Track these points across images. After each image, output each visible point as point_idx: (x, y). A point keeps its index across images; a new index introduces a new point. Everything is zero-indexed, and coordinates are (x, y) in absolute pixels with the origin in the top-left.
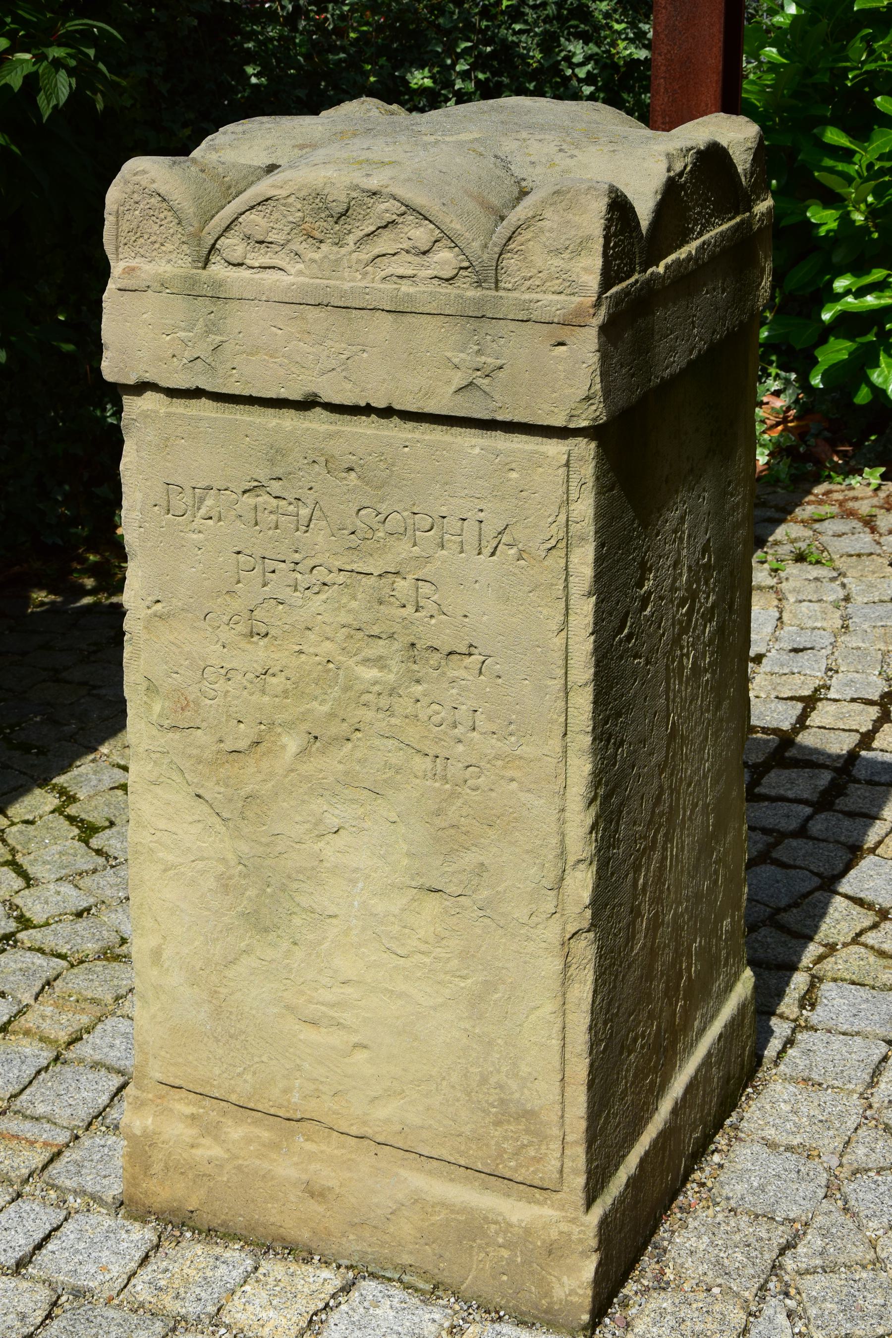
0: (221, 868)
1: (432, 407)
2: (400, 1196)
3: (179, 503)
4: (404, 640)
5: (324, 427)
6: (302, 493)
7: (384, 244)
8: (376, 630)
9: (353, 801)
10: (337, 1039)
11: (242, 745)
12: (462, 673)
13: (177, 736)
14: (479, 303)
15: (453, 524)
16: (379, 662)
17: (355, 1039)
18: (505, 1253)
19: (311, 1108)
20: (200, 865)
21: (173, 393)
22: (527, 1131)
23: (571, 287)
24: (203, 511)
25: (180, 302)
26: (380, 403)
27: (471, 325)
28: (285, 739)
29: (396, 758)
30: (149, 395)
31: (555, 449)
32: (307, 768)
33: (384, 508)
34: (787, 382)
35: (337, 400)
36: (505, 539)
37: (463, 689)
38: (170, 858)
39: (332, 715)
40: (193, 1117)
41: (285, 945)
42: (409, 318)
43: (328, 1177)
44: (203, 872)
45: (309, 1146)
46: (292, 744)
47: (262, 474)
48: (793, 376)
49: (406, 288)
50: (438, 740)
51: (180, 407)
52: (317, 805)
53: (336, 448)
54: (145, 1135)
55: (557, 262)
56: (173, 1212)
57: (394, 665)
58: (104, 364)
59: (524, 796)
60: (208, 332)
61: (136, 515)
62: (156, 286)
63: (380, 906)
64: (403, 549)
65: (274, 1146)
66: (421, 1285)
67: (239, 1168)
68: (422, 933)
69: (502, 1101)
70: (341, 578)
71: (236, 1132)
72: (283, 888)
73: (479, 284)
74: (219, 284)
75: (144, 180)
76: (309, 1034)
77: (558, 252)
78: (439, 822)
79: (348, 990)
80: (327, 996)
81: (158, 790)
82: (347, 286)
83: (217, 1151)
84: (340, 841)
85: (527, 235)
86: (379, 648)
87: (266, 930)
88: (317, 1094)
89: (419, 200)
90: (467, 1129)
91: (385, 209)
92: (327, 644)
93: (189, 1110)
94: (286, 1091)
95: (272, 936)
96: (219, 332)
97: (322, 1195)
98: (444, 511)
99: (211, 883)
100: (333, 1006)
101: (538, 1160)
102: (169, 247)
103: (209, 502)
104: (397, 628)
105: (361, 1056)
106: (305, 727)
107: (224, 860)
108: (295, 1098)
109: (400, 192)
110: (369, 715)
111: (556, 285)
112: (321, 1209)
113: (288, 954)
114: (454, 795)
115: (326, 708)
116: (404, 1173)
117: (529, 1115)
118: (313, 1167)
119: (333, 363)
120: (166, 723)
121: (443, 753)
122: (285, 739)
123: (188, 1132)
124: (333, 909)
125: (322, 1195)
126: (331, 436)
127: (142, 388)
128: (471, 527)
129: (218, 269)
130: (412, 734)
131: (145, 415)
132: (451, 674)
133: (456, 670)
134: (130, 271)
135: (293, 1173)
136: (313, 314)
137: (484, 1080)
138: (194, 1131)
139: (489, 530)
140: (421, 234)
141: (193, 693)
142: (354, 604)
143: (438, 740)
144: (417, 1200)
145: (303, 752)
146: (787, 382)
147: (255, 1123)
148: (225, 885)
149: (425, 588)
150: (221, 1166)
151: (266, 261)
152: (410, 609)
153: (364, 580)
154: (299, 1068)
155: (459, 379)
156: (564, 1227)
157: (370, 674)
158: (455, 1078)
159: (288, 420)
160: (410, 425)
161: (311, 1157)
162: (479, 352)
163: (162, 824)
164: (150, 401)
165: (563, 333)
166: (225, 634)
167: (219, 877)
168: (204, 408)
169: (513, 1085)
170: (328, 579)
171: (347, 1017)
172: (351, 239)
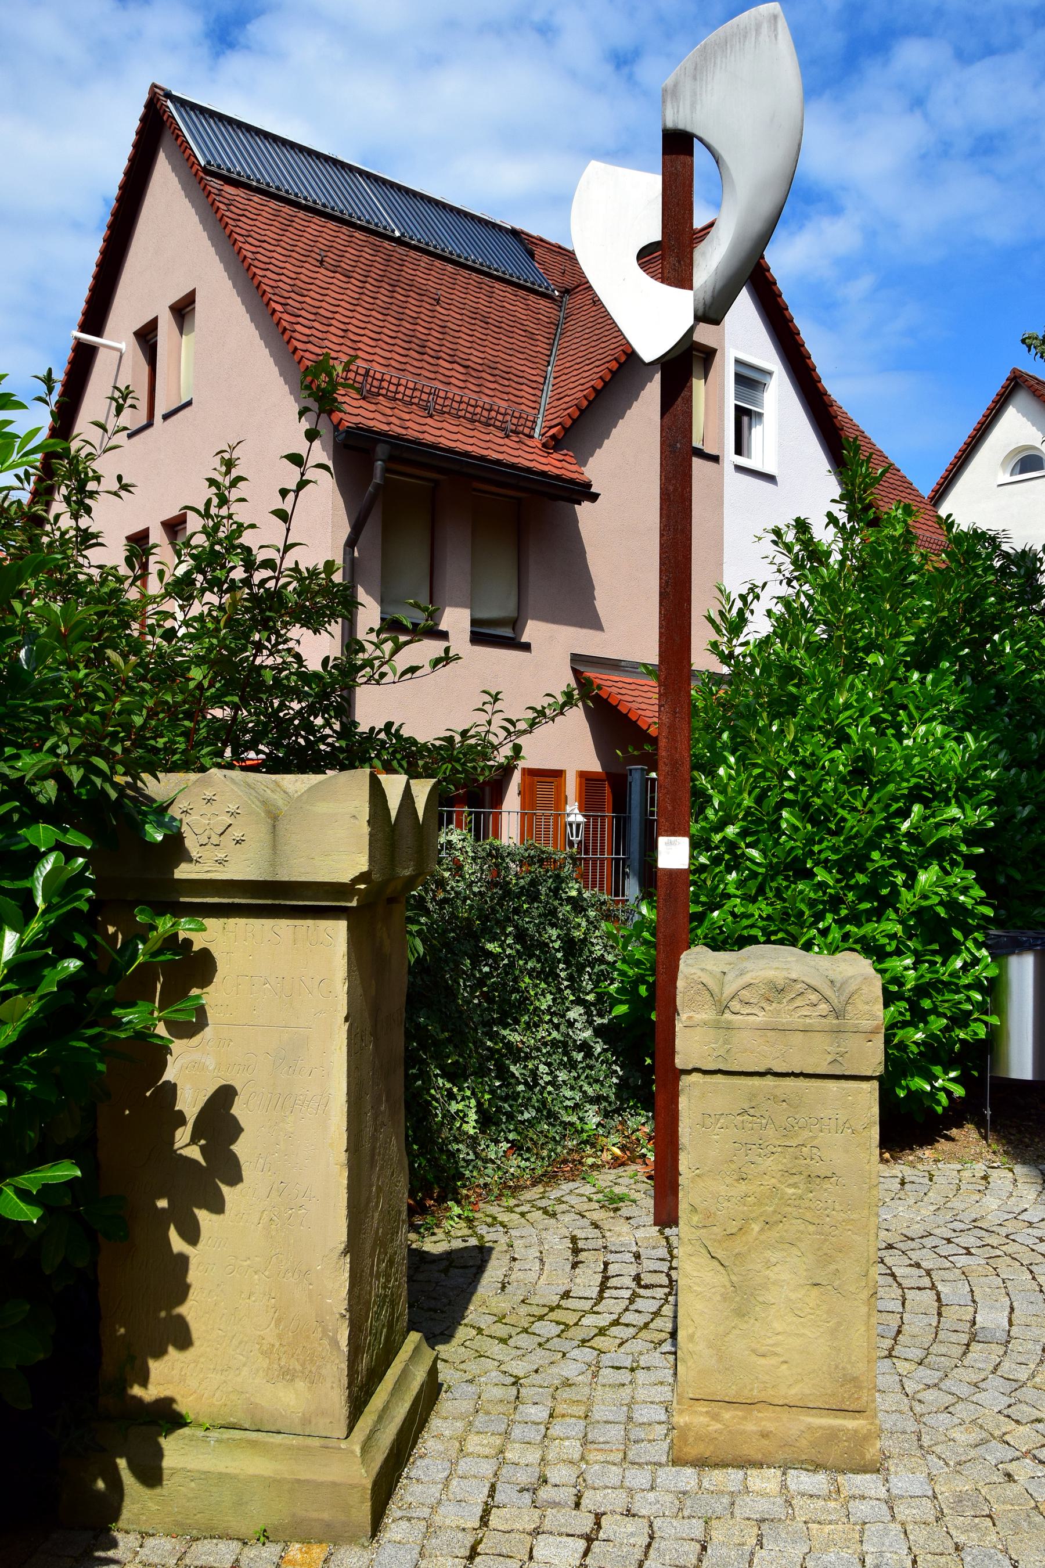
0: (723, 1290)
1: (819, 1071)
2: (802, 1428)
3: (708, 1121)
4: (806, 1174)
5: (772, 1083)
6: (764, 1113)
7: (799, 1002)
8: (794, 1171)
9: (783, 1250)
10: (773, 1361)
11: (733, 1231)
12: (829, 1186)
13: (704, 1231)
14: (838, 1025)
15: (826, 1121)
16: (794, 1185)
17: (782, 1359)
18: (846, 1444)
19: (763, 1396)
20: (713, 1290)
21: (706, 1072)
22: (855, 1386)
23: (875, 1017)
24: (719, 1125)
25: (712, 1031)
26: (797, 1071)
27: (836, 1034)
28: (753, 1226)
29: (802, 1228)
30: (694, 1074)
31: (865, 1085)
32: (762, 1238)
33: (797, 1116)
34: (648, 1117)
35: (779, 1071)
36: (847, 1125)
37: (830, 1193)
38: (699, 1289)
39: (775, 1211)
40: (707, 1412)
41: (752, 1321)
42: (809, 1034)
43: (770, 1426)
44: (714, 1294)
45: (760, 1415)
46: (756, 1227)
47: (746, 1106)
48: (650, 1114)
49: (808, 1020)
50: (819, 1217)
51: (708, 1078)
52: (768, 1254)
53: (778, 1092)
54: (686, 1425)
55: (867, 1007)
56: (698, 1460)
57: (801, 1186)
58: (677, 1061)
59: (855, 1237)
60: (725, 1044)
61: (687, 1130)
62: (702, 1024)
63: (793, 1296)
64: (806, 1134)
65: (745, 1418)
66: (810, 1468)
67: (730, 1432)
68: (811, 1305)
69: (844, 1375)
70: (779, 1149)
71: (727, 1415)
72: (752, 1294)
73: (837, 1018)
74: (729, 1022)
75: (695, 977)
76: (762, 1361)
77: (868, 1003)
78: (820, 1253)
79: (779, 1337)
80: (770, 1341)
81: (693, 1258)
82: (784, 1021)
83: (719, 1426)
84: (775, 1269)
85: (856, 996)
86: (795, 1179)
87: (744, 1316)
88: (765, 1389)
89: (813, 983)
90: (829, 1391)
91: (800, 987)
92: (773, 1180)
93: (705, 1410)
94: (752, 1390)
95: (746, 1318)
96: (729, 1044)
97: (767, 1435)
98: (822, 1115)
99: (719, 1298)
100: (772, 1346)
101: (858, 1399)
102: (706, 1007)
103: (722, 1121)
104: (803, 1169)
105: (784, 1367)
106: (763, 1218)
107: (724, 1286)
108: (755, 1393)
109: (806, 980)
110: (790, 1209)
111: (867, 1017)
112: (767, 1442)
113: (753, 1325)
114: (826, 1240)
115: (772, 1209)
116: (802, 1418)
117: (855, 1379)
118: (763, 1423)
119: (778, 1055)
120: (700, 1225)
121: (821, 1222)
122: (753, 1226)
123: (704, 1420)
124: (773, 1301)
125: (767, 1435)
126: (776, 1087)
127: (689, 1072)
128: (833, 1121)
129: (728, 1015)
130: (808, 1216)
131: (694, 1083)
132: (825, 1187)
133: (827, 1185)
134: (690, 1018)
135: (754, 1428)
136: (770, 1033)
137: (837, 1367)
138: (708, 1419)
139: (840, 1122)
140: (814, 997)
141: (713, 1209)
142: (785, 1160)
143: (819, 1217)
144: (810, 1428)
145: (762, 1230)
146: (648, 1117)
147: (736, 1409)
148: (725, 1298)
149: (815, 1150)
150: (721, 1433)
151: (749, 1011)
152: (809, 1160)
153: (789, 1149)
154: (757, 1378)
155: (830, 1058)
156: (869, 1427)
157: (791, 1191)
158: (825, 1368)
159: (756, 1081)
160: (807, 1080)
161: (762, 1419)
162: (838, 1046)
163: (695, 1274)
164: (695, 1077)
165: (871, 1037)
166: (728, 1180)
167: (721, 1295)
168: (719, 1077)
169: (849, 1367)
170: (774, 1150)
171: (778, 1350)
172: (785, 1001)
